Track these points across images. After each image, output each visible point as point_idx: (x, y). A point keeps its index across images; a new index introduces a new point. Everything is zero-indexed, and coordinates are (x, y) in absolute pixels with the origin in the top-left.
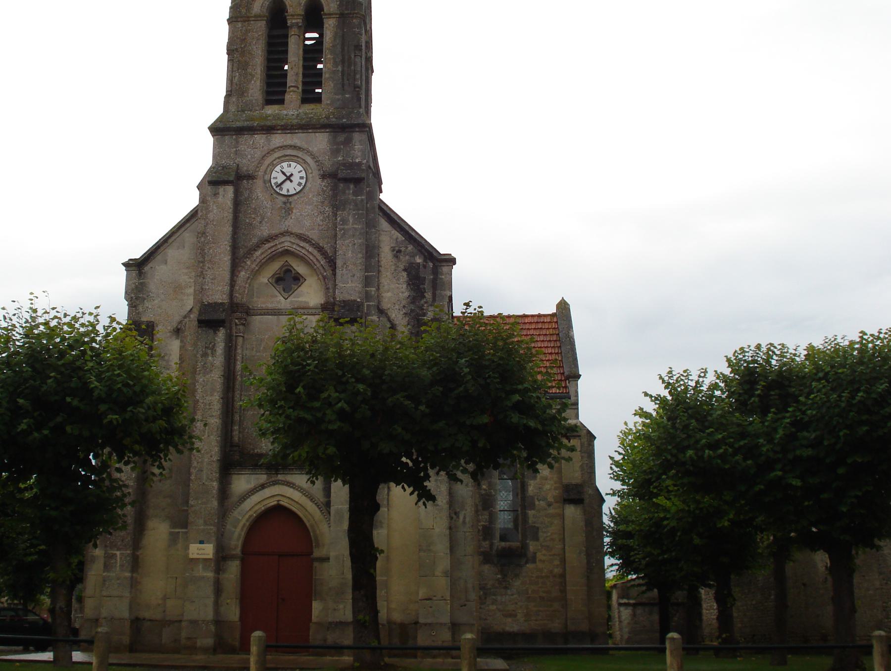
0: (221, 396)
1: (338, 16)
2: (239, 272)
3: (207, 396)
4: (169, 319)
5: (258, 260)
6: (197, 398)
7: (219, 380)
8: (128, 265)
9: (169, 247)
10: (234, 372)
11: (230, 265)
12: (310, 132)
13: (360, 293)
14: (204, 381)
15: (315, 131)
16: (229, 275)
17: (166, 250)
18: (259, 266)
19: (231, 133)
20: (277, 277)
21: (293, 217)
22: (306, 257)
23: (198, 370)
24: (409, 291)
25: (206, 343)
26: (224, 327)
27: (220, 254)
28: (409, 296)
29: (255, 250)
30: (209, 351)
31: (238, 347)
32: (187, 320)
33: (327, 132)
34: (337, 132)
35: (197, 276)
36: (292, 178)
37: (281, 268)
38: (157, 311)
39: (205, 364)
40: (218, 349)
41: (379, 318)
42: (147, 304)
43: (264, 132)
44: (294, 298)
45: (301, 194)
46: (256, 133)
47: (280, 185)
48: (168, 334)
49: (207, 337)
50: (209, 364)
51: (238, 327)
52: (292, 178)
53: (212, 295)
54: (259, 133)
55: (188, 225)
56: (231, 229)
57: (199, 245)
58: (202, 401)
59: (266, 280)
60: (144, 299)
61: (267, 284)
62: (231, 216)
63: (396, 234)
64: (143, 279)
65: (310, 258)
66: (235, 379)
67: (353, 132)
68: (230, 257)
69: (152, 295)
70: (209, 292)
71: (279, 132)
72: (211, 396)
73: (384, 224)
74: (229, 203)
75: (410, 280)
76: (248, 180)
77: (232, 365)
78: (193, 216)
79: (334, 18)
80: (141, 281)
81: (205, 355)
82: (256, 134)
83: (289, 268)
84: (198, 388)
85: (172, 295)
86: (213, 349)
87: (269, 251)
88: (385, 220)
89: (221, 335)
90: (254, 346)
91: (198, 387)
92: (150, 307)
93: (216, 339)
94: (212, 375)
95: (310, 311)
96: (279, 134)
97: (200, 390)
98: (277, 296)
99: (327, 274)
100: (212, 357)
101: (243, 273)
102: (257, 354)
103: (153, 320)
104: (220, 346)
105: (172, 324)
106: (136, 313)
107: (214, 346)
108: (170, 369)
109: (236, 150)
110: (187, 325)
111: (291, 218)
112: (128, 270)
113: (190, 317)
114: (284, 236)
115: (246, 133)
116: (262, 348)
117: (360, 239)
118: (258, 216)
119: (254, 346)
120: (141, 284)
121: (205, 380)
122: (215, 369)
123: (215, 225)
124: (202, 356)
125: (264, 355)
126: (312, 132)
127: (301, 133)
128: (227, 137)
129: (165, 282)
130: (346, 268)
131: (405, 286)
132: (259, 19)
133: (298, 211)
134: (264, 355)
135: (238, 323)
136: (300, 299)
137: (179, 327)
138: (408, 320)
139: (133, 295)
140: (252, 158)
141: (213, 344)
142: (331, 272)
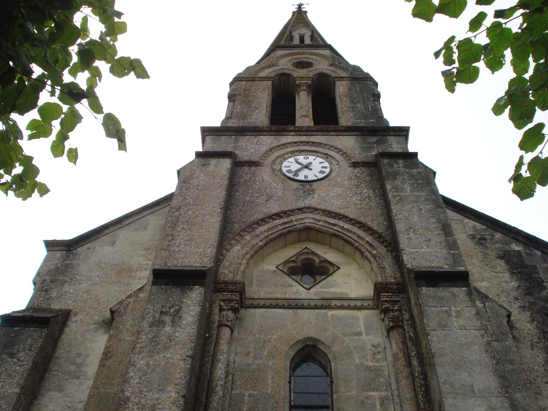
0: (190, 353)
1: (350, 79)
2: (232, 246)
3: (150, 391)
4: (100, 307)
5: (262, 236)
6: (127, 394)
7: (181, 363)
8: (50, 245)
9: (122, 229)
10: (210, 381)
11: (219, 228)
12: (331, 135)
13: (445, 258)
14: (147, 365)
15: (338, 133)
16: (216, 236)
17: (118, 231)
18: (264, 241)
19: (230, 133)
20: (290, 267)
21: (315, 197)
22: (341, 234)
23: (139, 346)
24: (516, 280)
25: (163, 307)
26: (202, 285)
27: (205, 215)
28: (519, 286)
29: (259, 225)
30: (167, 319)
31: (222, 342)
32: (132, 300)
33: (353, 135)
34: (366, 135)
35: (161, 249)
36: (311, 167)
37: (299, 254)
38: (82, 296)
39: (155, 336)
40: (185, 315)
41: (483, 303)
42: (66, 287)
43: (273, 134)
44: (322, 288)
45: (325, 181)
46: (262, 134)
47: (296, 173)
48: (92, 327)
49: (168, 298)
50: (164, 338)
51: (224, 313)
52: (311, 167)
53: (183, 258)
54: (265, 134)
55: (157, 208)
56: (224, 193)
57: (170, 218)
58: (137, 400)
59: (273, 268)
60: (65, 282)
61: (275, 271)
62: (225, 182)
63: (471, 223)
64: (71, 260)
65: (346, 235)
66: (210, 390)
67: (387, 136)
68: (219, 219)
69: (80, 278)
70: (180, 254)
71: (293, 133)
72: (159, 391)
73: (451, 214)
74: (224, 172)
75: (512, 267)
76: (250, 166)
77: (208, 365)
78: (168, 199)
79: (346, 80)
80: (67, 262)
81: (158, 323)
82: (262, 135)
83: (310, 256)
84: (132, 377)
85: (112, 278)
86: (177, 316)
87: (281, 228)
88: (451, 210)
89: (194, 296)
90: (252, 350)
91: (132, 374)
92: (71, 291)
93: (184, 300)
94: (169, 355)
95: (353, 304)
96: (292, 135)
97: (137, 380)
98: (291, 286)
99: (378, 252)
100: (172, 326)
101: (237, 248)
102: (257, 362)
103: (71, 307)
104: (192, 310)
105: (103, 313)
106: (45, 298)
107: (178, 311)
108: (82, 377)
109: (235, 146)
110: (130, 307)
111: (313, 198)
112: (51, 251)
113: (137, 297)
114: (304, 212)
115: (248, 134)
116: (265, 353)
117: (428, 205)
118: (262, 195)
119: (252, 350)
120: (67, 266)
121: (151, 362)
122: (175, 345)
123: (200, 189)
124: (152, 325)
125: (270, 364)
126: (334, 135)
127: (320, 135)
128: (223, 137)
129: (105, 263)
130: (414, 232)
131: (507, 275)
132: (265, 79)
133: (322, 191)
134: (270, 364)
135: (225, 307)
136: (332, 290)
137: (115, 308)
138: (531, 315)
139: (47, 278)
140: (255, 151)
141: (177, 307)
142: (385, 249)
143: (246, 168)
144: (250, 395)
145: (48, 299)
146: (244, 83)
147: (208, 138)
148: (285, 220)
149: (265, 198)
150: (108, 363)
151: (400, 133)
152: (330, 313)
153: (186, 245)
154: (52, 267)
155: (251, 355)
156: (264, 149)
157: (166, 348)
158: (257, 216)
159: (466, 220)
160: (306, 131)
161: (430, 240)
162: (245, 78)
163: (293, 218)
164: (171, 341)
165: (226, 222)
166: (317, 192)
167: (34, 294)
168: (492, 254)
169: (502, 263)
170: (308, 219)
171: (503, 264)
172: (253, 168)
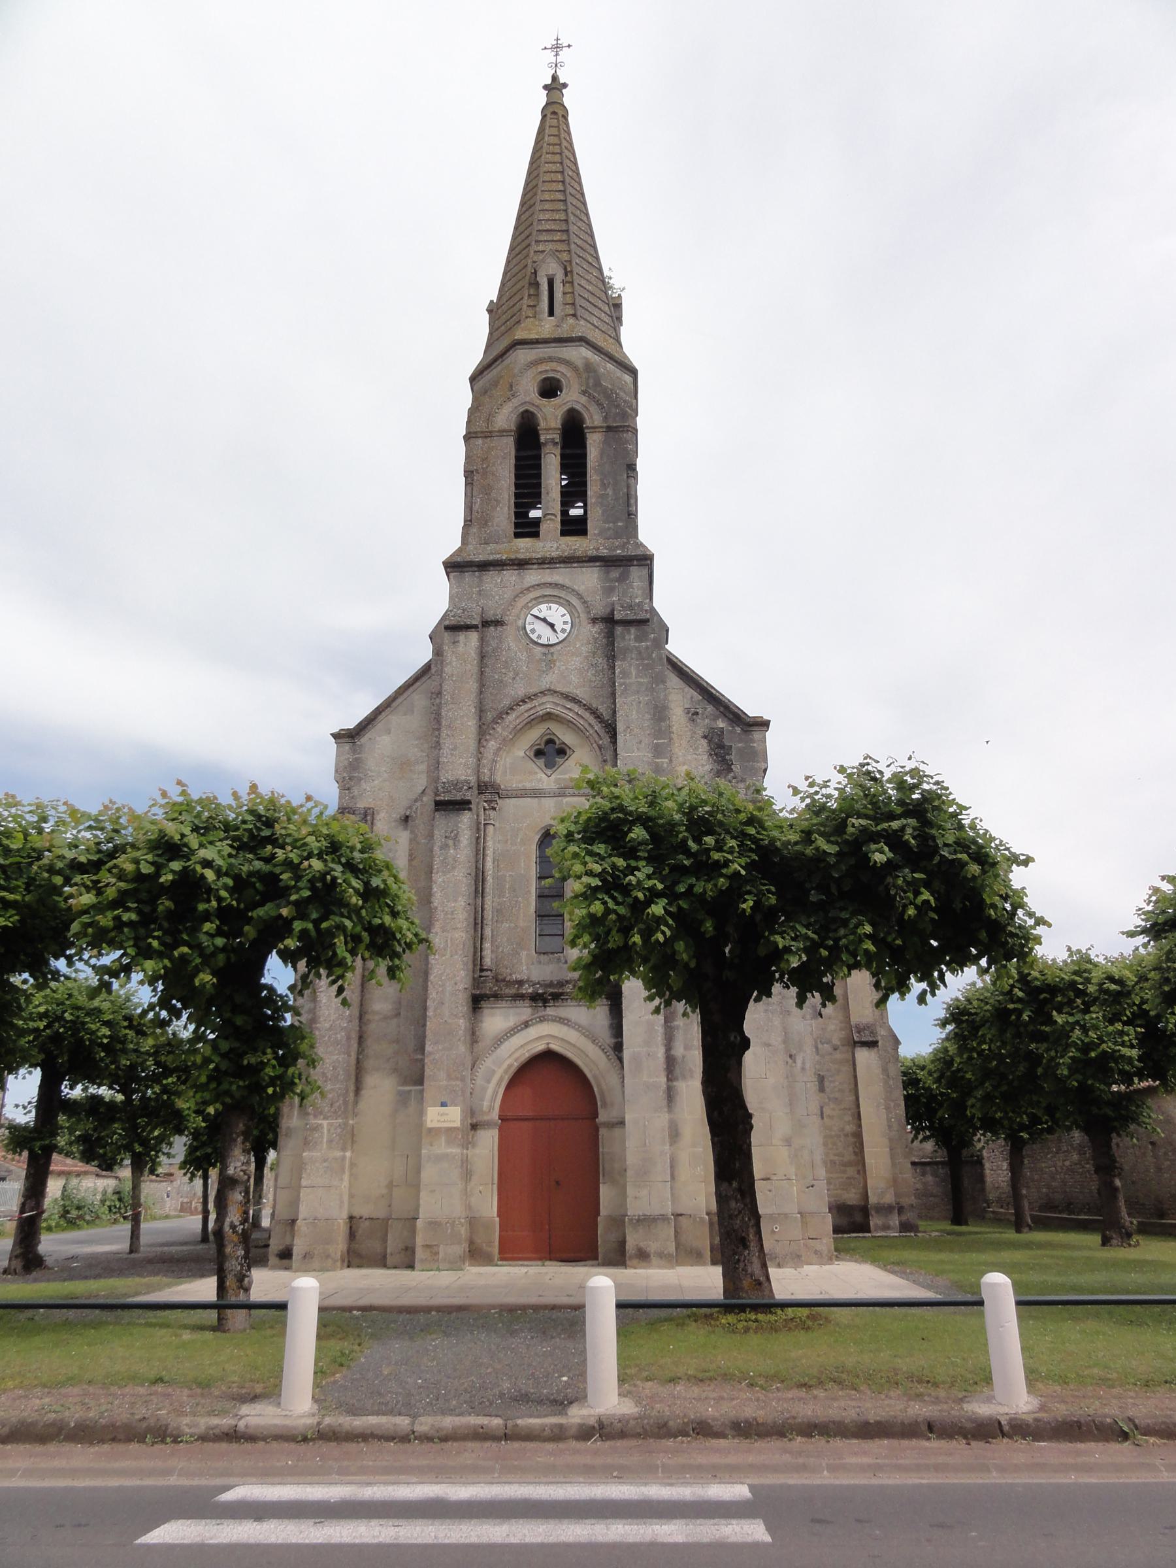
14: (444, 882)
15: (581, 565)
25: (446, 831)
30: (450, 842)
39: (445, 859)
42: (364, 785)
51: (487, 812)
71: (535, 566)
78: (426, 670)
87: (526, 715)
107: (456, 836)
117: (647, 695)
143: (492, 628)
144: (510, 875)
145: (353, 797)
146: (480, 441)
147: (452, 575)
148: (529, 706)
149: (511, 674)
150: (414, 863)
151: (643, 562)
152: (566, 800)
153: (452, 754)
154: (346, 763)
155: (509, 842)
156: (508, 595)
157: (454, 868)
158: (506, 702)
159: (687, 689)
160: (550, 563)
161: (641, 742)
162: (482, 432)
163: (535, 703)
164: (456, 861)
165: (481, 711)
166: (557, 664)
167: (340, 793)
168: (700, 732)
169: (704, 742)
170: (548, 704)
171: (705, 745)
172: (499, 628)
